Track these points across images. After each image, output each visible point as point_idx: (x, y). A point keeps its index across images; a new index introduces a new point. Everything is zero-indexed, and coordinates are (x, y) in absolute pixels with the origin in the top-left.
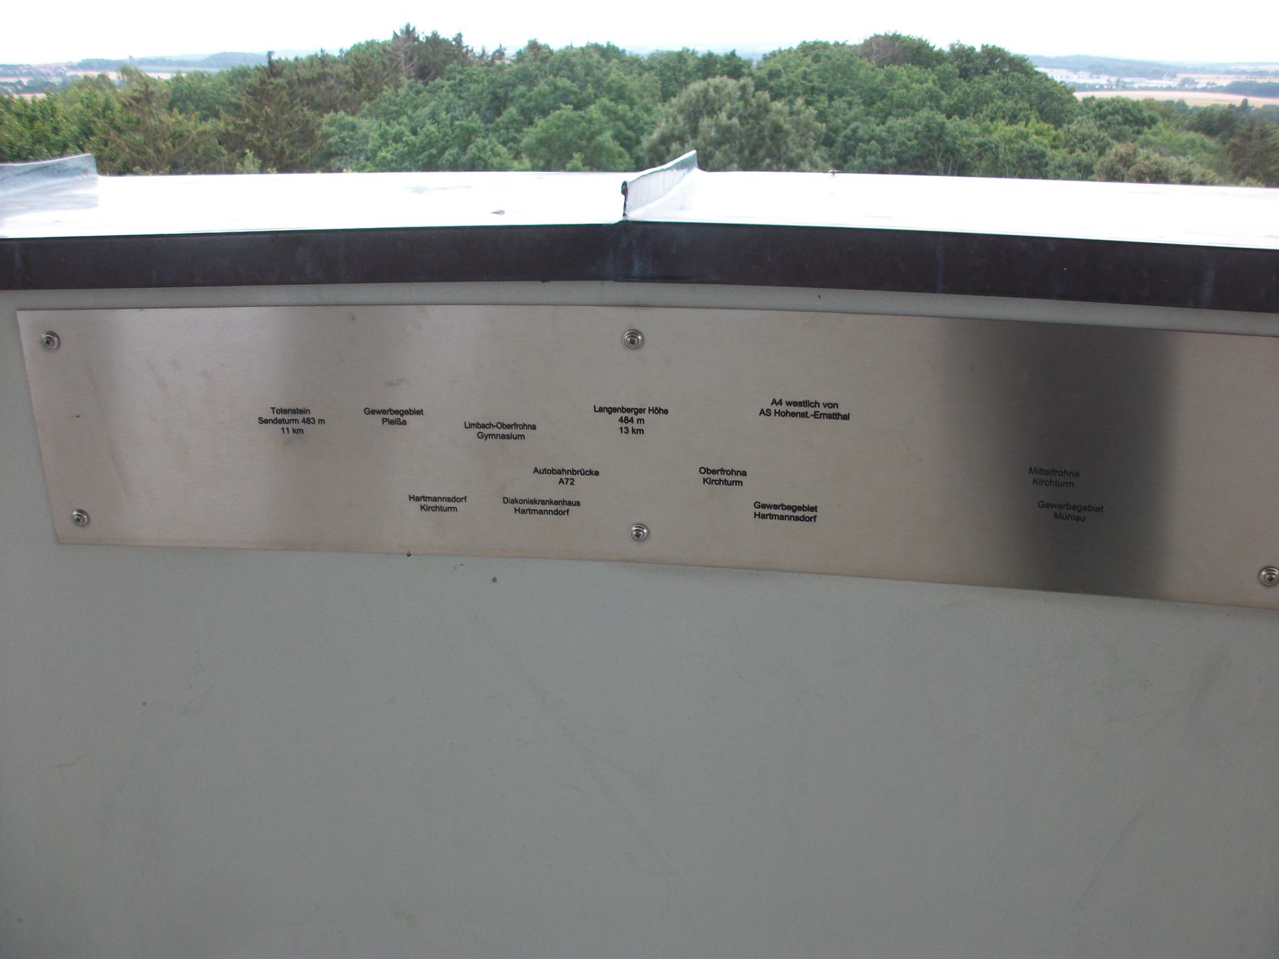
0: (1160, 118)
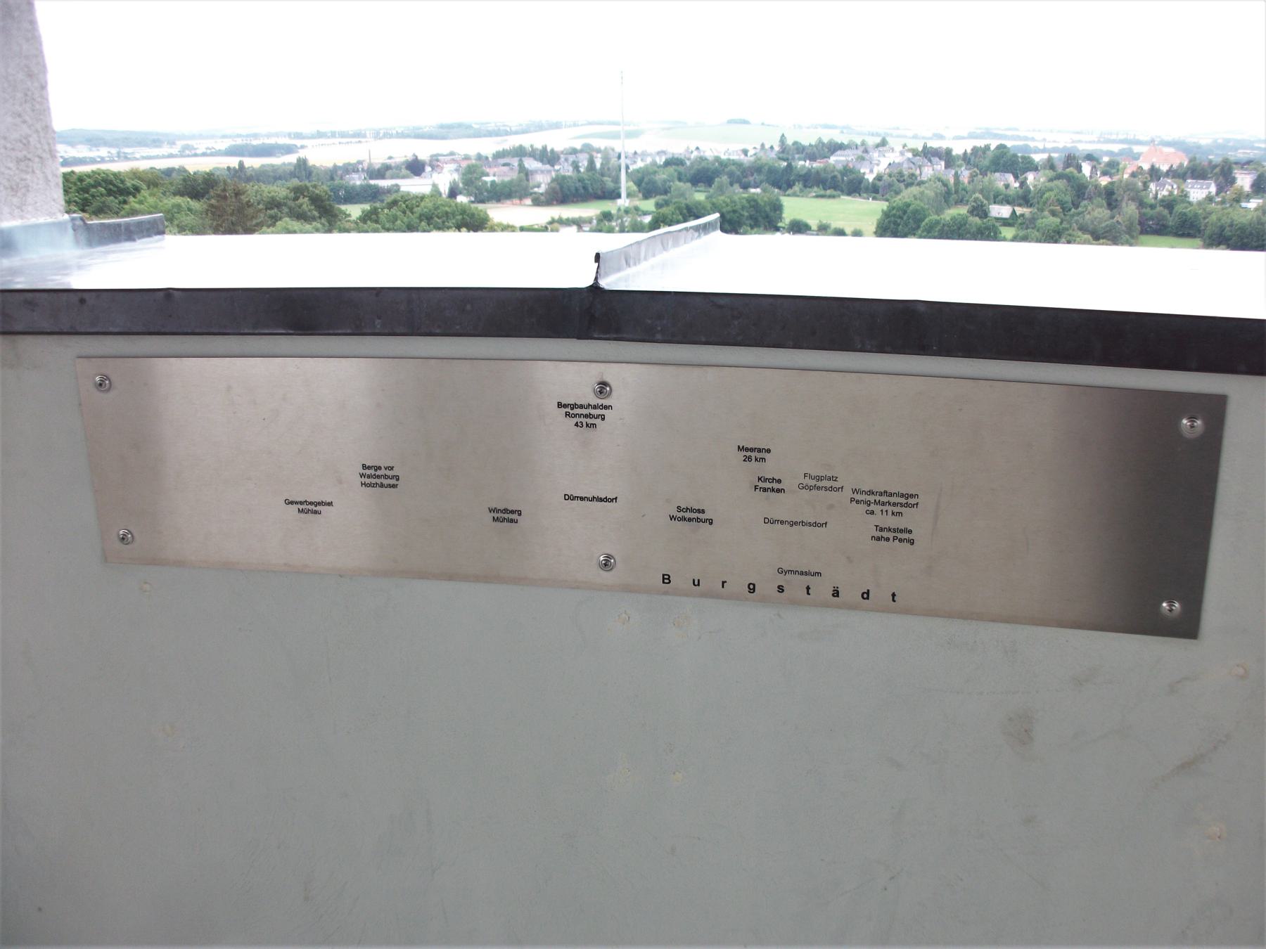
0: (144, 187)
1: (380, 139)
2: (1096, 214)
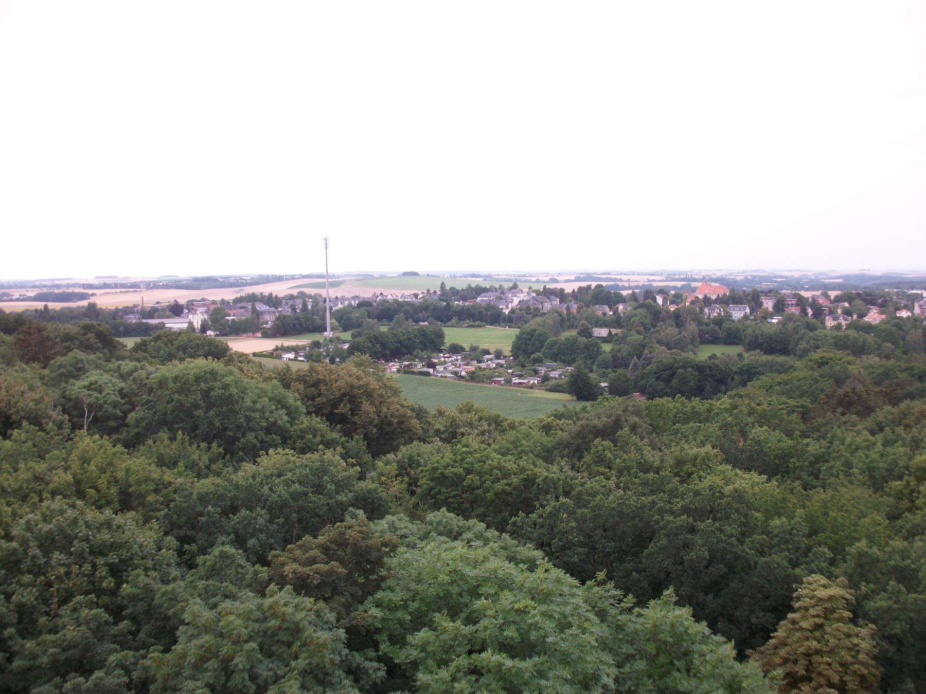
1: (151, 289)
2: (668, 331)
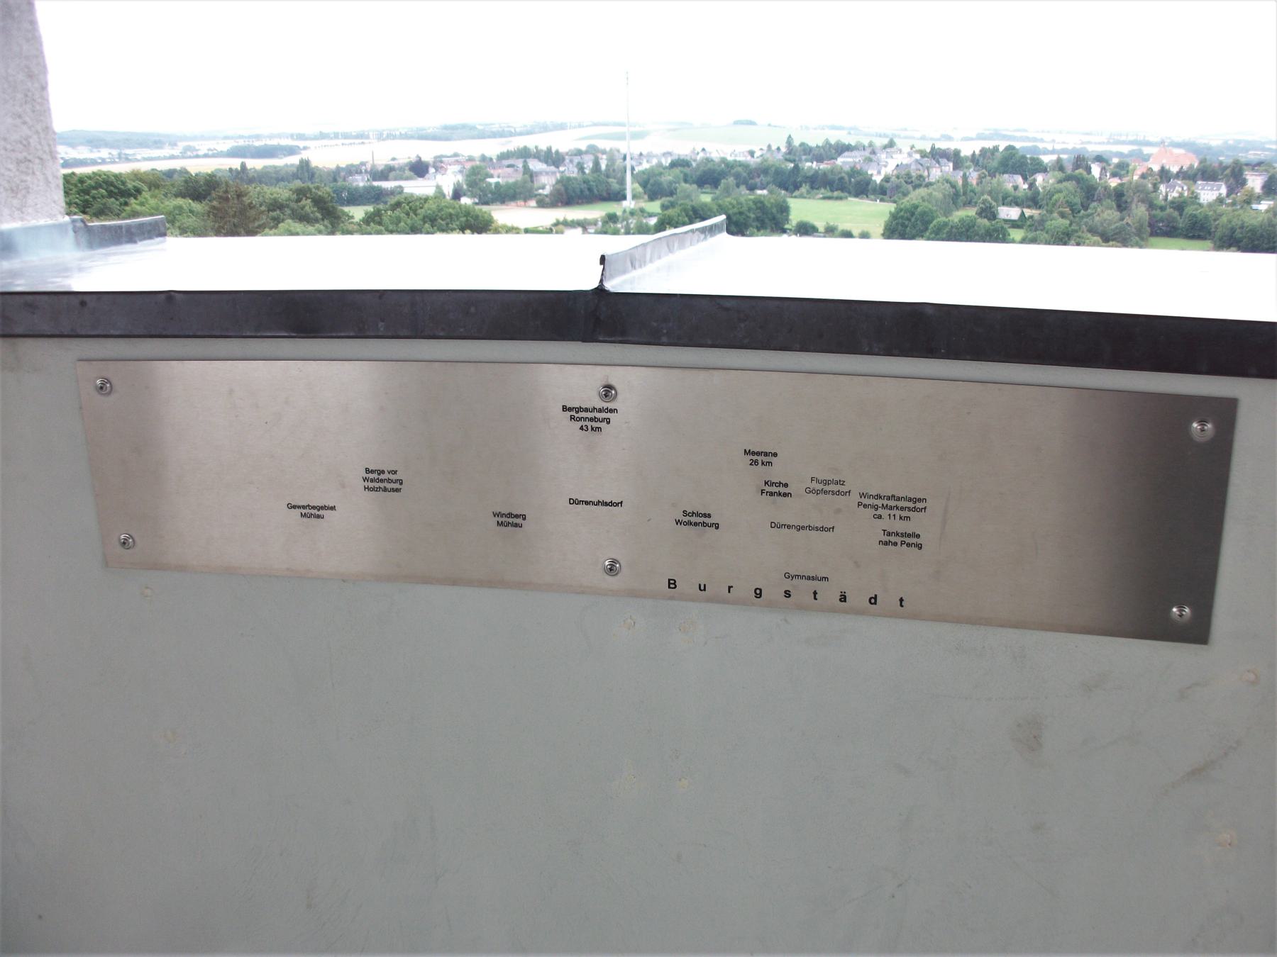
0: (146, 188)
1: (384, 140)
2: (1105, 215)
